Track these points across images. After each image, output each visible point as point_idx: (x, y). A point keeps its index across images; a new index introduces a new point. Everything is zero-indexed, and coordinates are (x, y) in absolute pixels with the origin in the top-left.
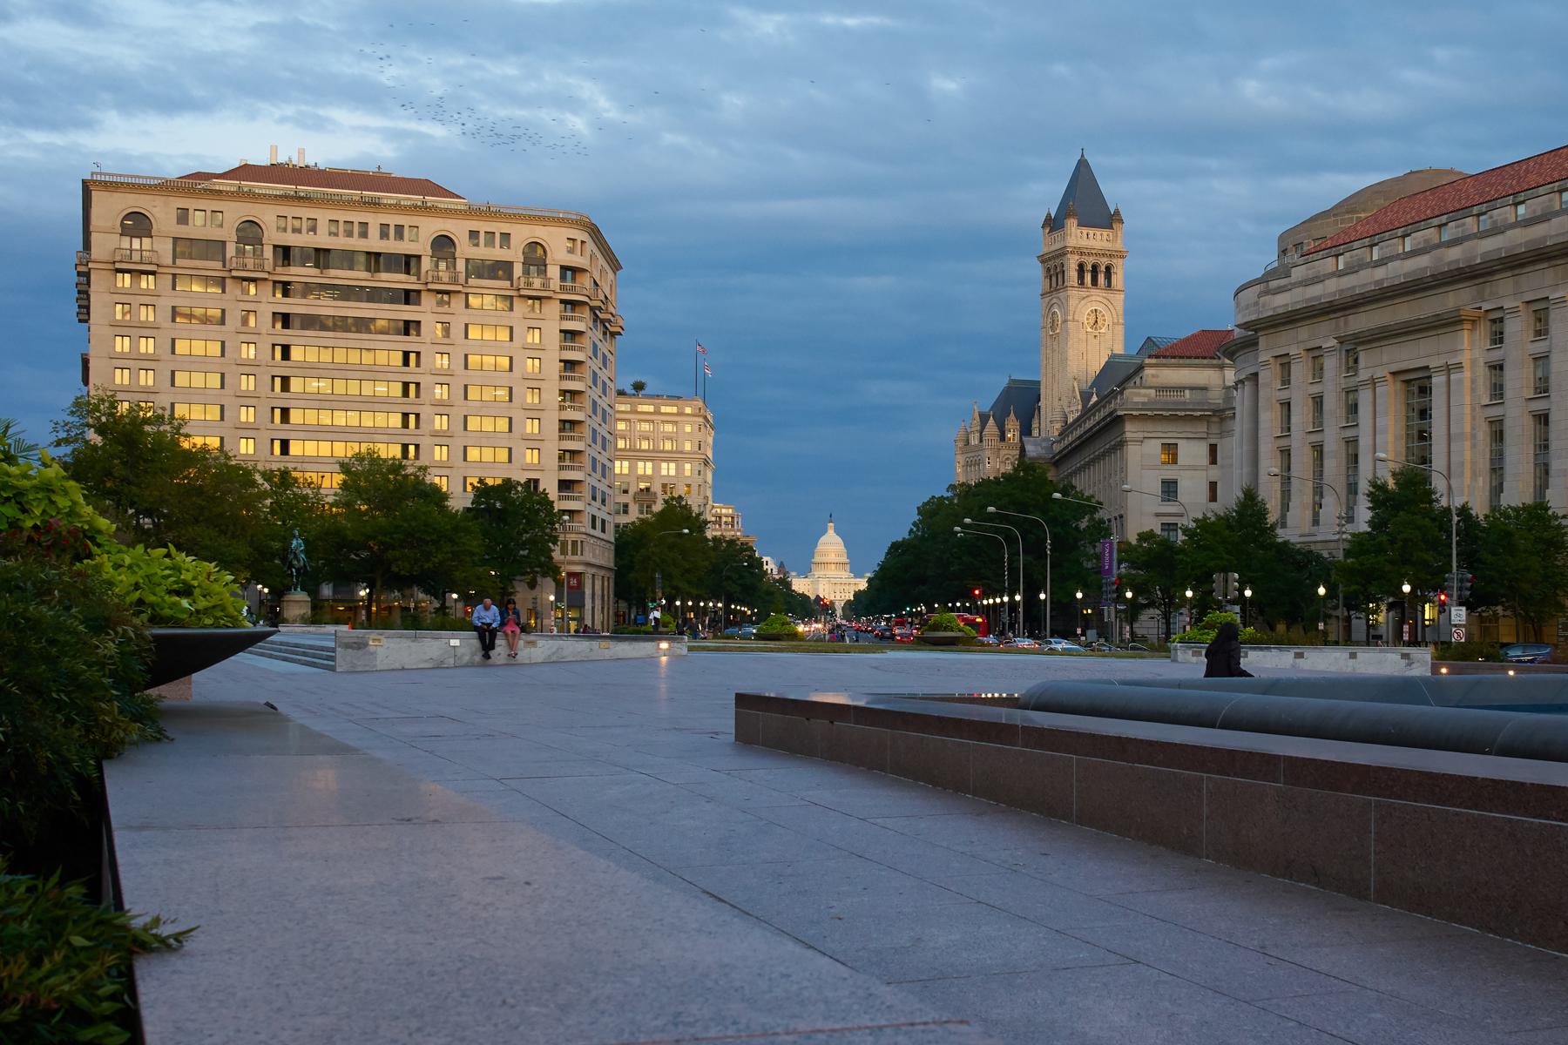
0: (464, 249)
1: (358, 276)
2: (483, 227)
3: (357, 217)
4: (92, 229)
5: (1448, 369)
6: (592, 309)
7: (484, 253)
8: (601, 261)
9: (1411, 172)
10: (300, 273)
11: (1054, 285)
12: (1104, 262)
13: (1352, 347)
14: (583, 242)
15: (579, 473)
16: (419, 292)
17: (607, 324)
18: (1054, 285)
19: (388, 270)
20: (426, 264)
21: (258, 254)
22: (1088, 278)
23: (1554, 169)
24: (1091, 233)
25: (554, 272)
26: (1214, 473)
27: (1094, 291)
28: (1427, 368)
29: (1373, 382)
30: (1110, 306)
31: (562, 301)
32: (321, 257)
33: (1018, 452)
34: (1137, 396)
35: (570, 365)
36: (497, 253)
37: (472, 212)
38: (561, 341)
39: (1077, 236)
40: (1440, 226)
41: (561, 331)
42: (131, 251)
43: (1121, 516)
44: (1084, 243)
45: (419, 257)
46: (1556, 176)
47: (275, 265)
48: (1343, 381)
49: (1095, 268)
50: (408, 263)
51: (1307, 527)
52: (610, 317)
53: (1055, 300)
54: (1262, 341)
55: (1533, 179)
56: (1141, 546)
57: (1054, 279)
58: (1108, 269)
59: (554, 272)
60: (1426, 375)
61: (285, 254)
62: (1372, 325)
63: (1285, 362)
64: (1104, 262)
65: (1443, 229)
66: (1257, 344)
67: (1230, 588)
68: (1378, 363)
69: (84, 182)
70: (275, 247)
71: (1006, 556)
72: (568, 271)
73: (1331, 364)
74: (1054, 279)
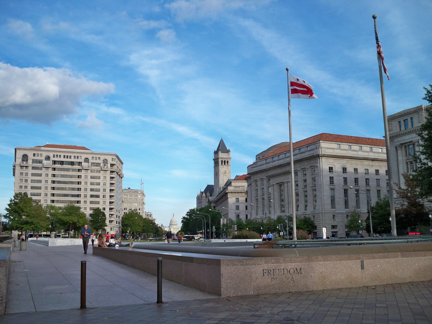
0: (91, 161)
1: (70, 166)
2: (95, 156)
4: (16, 158)
5: (288, 182)
6: (117, 173)
7: (94, 161)
8: (119, 162)
9: (282, 143)
10: (58, 166)
12: (226, 160)
13: (269, 178)
14: (115, 159)
15: (113, 206)
16: (81, 169)
17: (120, 175)
22: (223, 163)
23: (306, 142)
24: (224, 154)
25: (109, 165)
26: (246, 204)
27: (225, 166)
28: (283, 182)
29: (273, 185)
30: (228, 169)
31: (110, 171)
32: (62, 163)
33: (208, 200)
34: (230, 189)
35: (112, 184)
36: (98, 161)
37: (92, 153)
38: (110, 179)
39: (221, 155)
40: (285, 154)
41: (110, 177)
42: (324, 213)
43: (228, 213)
44: (222, 156)
46: (307, 144)
48: (268, 185)
49: (225, 162)
50: (80, 164)
51: (312, 210)
52: (121, 174)
53: (216, 168)
54: (252, 177)
55: (303, 144)
57: (216, 164)
58: (227, 161)
60: (283, 184)
61: (55, 162)
62: (272, 174)
63: (256, 181)
64: (226, 160)
65: (279, 156)
66: (251, 178)
67: (235, 228)
68: (274, 181)
69: (15, 149)
70: (52, 161)
71: (203, 222)
72: (112, 165)
73: (265, 182)
74: (216, 164)
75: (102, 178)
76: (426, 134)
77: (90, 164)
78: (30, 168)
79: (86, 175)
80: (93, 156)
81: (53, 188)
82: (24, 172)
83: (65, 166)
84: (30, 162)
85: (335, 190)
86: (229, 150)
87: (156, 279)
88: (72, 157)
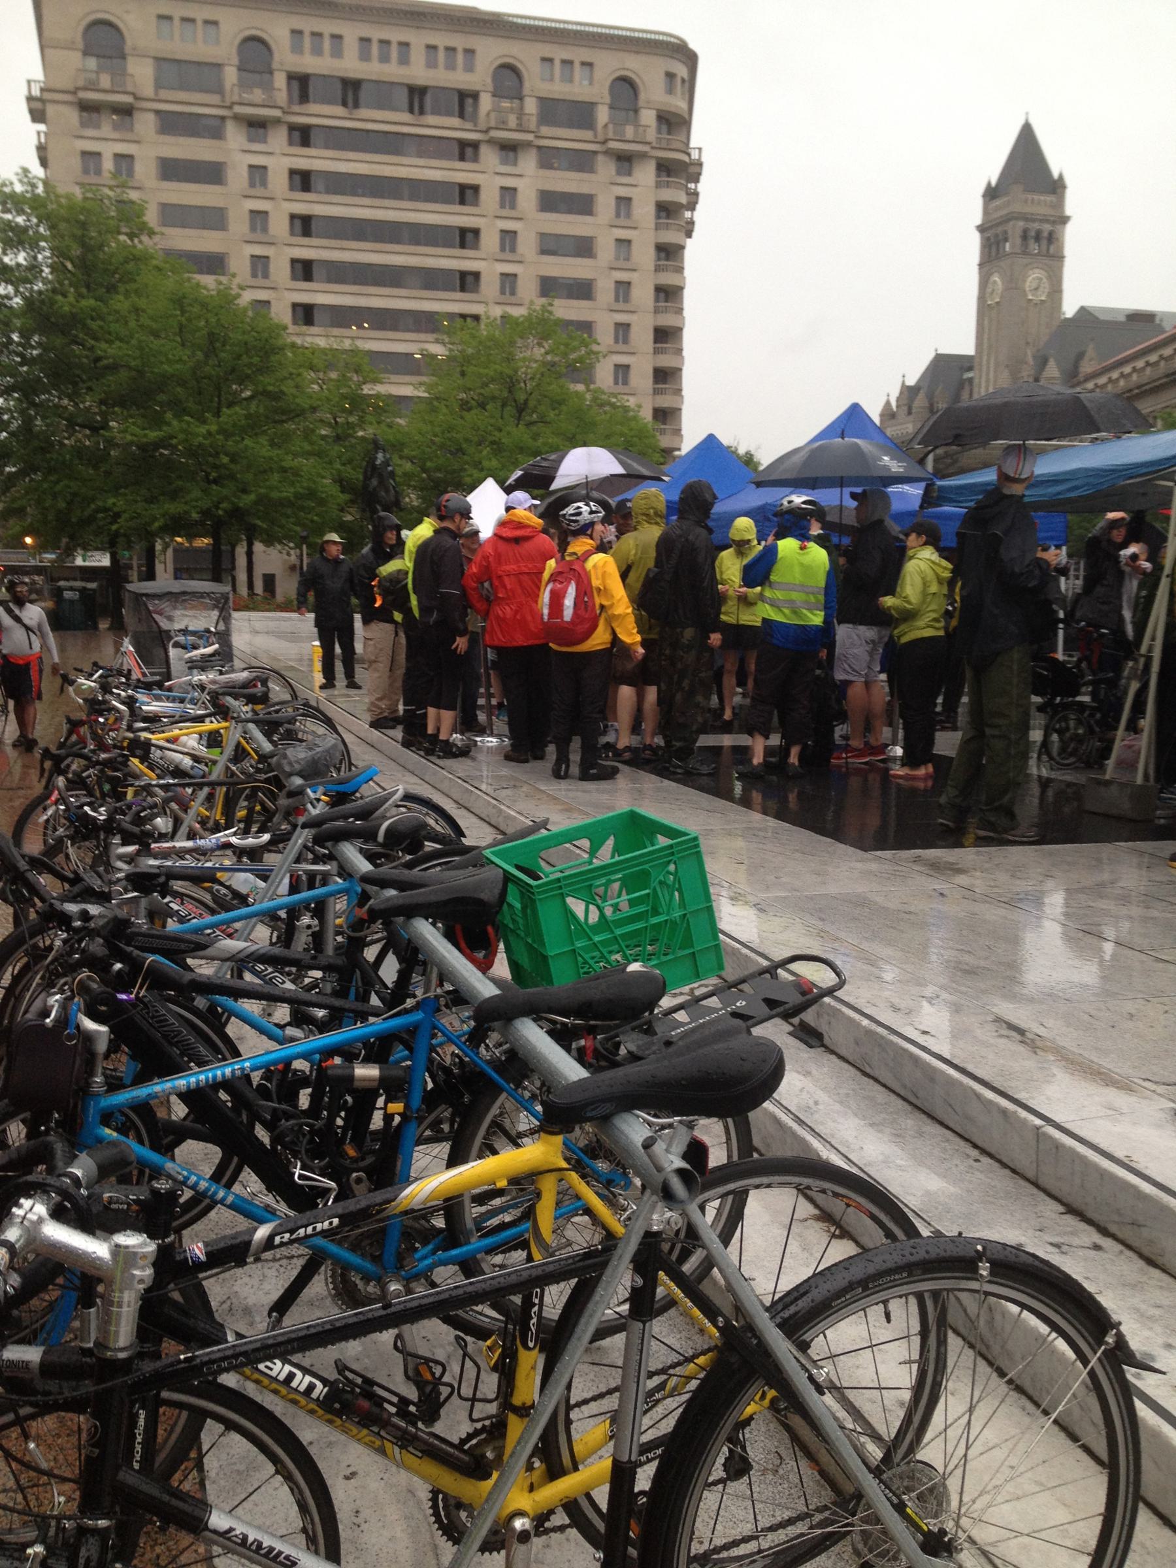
1: (396, 120)
2: (559, 53)
3: (395, 35)
7: (558, 89)
11: (993, 254)
18: (993, 254)
19: (436, 112)
20: (486, 102)
21: (268, 87)
25: (648, 117)
36: (460, 79)
45: (475, 96)
47: (290, 101)
50: (464, 101)
56: (37, 414)
59: (648, 117)
61: (302, 85)
75: (605, 206)
76: (638, 1028)
77: (531, 106)
78: (145, 123)
79: (510, 182)
80: (548, 50)
81: (304, 270)
82: (109, 150)
83: (373, 118)
84: (141, 73)
85: (596, 69)
86: (1061, 177)
87: (544, 1315)
88: (418, 55)
